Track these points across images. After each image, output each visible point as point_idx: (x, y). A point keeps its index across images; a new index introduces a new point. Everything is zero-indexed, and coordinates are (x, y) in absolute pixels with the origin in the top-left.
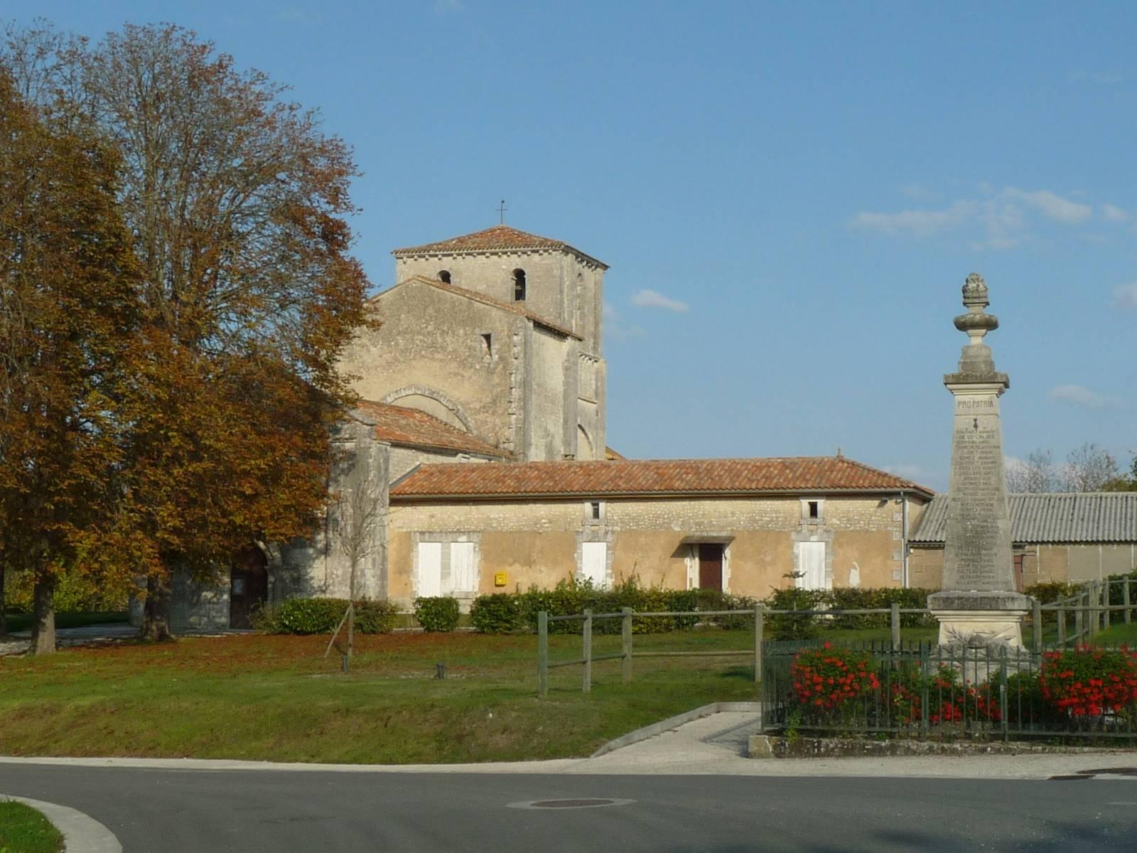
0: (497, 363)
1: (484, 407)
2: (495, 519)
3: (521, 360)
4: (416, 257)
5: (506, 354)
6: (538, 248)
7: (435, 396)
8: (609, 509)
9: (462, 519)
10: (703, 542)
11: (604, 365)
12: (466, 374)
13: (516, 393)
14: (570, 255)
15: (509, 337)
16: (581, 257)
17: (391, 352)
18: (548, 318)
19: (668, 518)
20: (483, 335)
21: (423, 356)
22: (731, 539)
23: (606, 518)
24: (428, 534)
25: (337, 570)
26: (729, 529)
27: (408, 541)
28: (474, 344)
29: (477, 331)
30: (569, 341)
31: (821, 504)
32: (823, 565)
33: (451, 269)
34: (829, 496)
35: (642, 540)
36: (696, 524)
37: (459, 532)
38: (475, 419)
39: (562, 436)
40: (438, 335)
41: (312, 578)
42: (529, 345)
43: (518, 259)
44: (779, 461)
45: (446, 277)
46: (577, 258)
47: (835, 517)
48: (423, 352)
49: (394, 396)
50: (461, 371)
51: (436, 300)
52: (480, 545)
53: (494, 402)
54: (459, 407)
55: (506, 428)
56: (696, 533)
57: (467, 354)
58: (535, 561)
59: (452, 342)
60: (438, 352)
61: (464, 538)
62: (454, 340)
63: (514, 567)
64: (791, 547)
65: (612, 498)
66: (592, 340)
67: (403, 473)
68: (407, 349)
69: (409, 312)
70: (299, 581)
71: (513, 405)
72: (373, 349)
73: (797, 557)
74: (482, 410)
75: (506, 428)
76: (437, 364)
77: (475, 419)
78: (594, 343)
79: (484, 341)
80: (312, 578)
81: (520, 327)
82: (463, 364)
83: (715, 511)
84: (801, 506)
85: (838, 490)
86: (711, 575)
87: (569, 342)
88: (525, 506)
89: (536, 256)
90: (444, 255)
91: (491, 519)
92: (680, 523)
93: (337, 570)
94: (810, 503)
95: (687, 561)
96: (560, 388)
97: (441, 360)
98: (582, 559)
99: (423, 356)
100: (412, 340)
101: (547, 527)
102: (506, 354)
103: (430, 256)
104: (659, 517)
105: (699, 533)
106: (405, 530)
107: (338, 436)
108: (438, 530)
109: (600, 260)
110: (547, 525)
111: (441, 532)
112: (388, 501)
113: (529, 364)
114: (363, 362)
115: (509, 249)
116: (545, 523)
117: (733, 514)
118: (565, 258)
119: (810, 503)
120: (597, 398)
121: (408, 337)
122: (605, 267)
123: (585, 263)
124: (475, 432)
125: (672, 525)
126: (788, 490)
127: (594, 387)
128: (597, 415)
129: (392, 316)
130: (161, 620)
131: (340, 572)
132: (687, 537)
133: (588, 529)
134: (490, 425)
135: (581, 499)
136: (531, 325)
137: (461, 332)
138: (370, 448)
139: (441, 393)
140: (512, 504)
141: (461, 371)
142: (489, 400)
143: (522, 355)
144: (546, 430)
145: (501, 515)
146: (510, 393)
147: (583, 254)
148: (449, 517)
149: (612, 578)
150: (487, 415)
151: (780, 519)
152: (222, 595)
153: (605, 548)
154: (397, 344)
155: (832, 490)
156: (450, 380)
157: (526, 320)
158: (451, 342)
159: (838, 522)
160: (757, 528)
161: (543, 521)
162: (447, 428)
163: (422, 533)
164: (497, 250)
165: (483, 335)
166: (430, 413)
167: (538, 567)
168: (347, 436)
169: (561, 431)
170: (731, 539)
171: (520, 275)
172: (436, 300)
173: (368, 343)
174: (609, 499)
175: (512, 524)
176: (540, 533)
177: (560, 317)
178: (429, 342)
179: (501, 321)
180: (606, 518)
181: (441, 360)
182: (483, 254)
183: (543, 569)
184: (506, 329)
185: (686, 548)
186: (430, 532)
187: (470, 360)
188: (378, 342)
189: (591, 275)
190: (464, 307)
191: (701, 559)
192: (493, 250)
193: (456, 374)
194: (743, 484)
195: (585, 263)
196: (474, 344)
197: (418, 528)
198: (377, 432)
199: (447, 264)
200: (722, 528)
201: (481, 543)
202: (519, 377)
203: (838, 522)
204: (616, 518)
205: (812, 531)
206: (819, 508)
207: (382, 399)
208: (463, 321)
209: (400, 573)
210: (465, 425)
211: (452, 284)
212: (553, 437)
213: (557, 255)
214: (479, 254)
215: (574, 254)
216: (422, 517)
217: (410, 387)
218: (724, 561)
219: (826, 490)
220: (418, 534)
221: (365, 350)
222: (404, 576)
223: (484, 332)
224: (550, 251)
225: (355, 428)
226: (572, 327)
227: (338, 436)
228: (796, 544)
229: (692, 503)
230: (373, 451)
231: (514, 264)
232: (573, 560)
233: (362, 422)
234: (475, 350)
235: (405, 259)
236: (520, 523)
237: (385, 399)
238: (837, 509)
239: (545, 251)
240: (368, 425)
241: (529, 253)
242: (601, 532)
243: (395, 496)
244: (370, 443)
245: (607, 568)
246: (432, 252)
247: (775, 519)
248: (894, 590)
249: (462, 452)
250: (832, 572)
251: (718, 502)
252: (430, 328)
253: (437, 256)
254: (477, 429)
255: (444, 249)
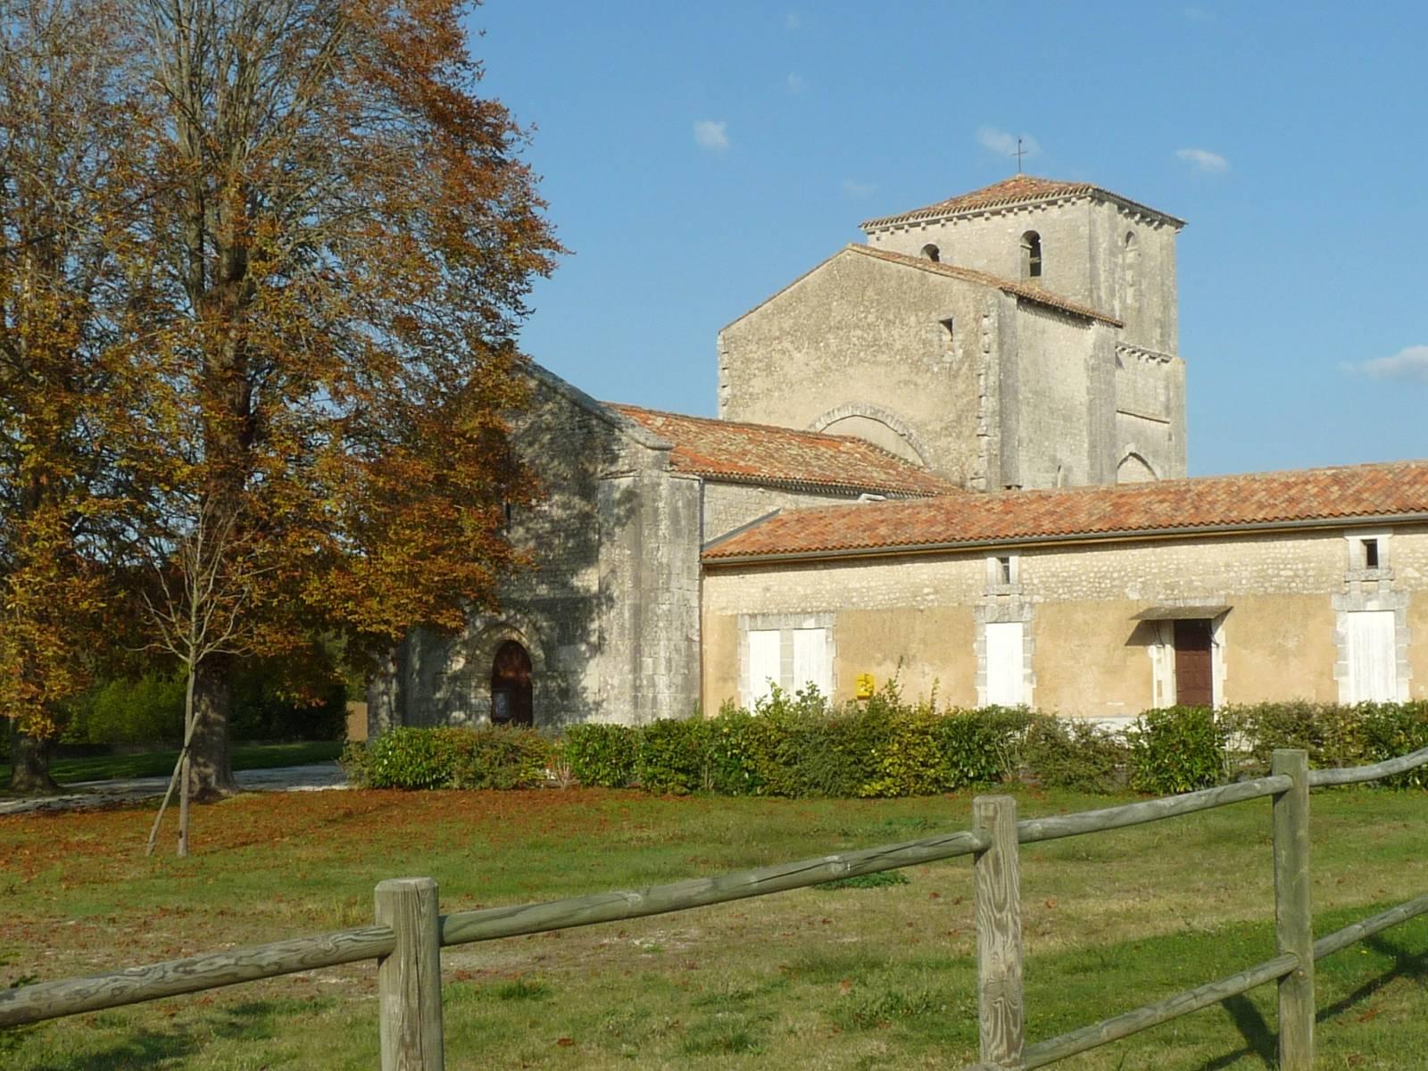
0: (962, 362)
1: (946, 429)
2: (855, 590)
3: (994, 354)
4: (892, 229)
5: (973, 347)
6: (1055, 197)
7: (879, 416)
8: (1025, 566)
9: (809, 592)
10: (1154, 617)
11: (1181, 366)
12: (919, 381)
13: (989, 404)
14: (1107, 204)
15: (977, 320)
16: (1127, 207)
17: (819, 358)
18: (1072, 298)
19: (1120, 578)
20: (942, 322)
21: (862, 360)
22: (1224, 613)
23: (1020, 581)
24: (761, 618)
25: (612, 677)
26: (1222, 593)
27: (734, 630)
28: (929, 336)
29: (934, 316)
30: (1096, 326)
31: (1384, 541)
32: (1392, 653)
33: (939, 241)
34: (1399, 527)
35: (1079, 617)
36: (1166, 586)
37: (804, 612)
38: (934, 447)
39: (1087, 468)
40: (882, 327)
41: (585, 689)
42: (1009, 331)
43: (1029, 218)
44: (1329, 472)
45: (933, 252)
46: (1121, 208)
47: (1411, 565)
48: (862, 354)
49: (825, 420)
50: (915, 378)
51: (878, 277)
52: (835, 632)
53: (959, 420)
54: (912, 431)
55: (975, 457)
56: (1164, 601)
57: (921, 351)
58: (914, 656)
59: (901, 336)
60: (883, 353)
61: (810, 623)
62: (903, 333)
63: (883, 667)
64: (1331, 622)
65: (1030, 548)
66: (1159, 331)
67: (738, 525)
68: (840, 351)
69: (842, 298)
70: (568, 696)
71: (983, 422)
72: (797, 355)
73: (1343, 640)
74: (944, 432)
75: (975, 457)
76: (882, 370)
77: (934, 447)
78: (1162, 335)
79: (946, 330)
80: (585, 689)
81: (992, 305)
82: (916, 365)
83: (1196, 562)
84: (1347, 549)
85: (1412, 514)
86: (1194, 681)
87: (1094, 332)
88: (899, 567)
89: (1054, 210)
90: (928, 223)
91: (849, 591)
92: (1139, 585)
93: (612, 677)
94: (1364, 541)
95: (1153, 650)
96: (1082, 397)
97: (887, 364)
98: (985, 652)
99: (862, 360)
100: (848, 338)
101: (932, 601)
102: (973, 347)
103: (911, 225)
104: (1104, 577)
105: (1171, 603)
106: (730, 613)
107: (613, 469)
108: (775, 611)
109: (1165, 213)
110: (932, 597)
111: (779, 614)
112: (697, 569)
113: (1009, 359)
114: (785, 375)
115: (1016, 204)
116: (928, 594)
117: (1227, 565)
118: (1098, 208)
119: (1364, 541)
120: (1168, 414)
121: (841, 333)
122: (1179, 224)
123: (1137, 217)
124: (934, 466)
125: (1127, 590)
126: (1321, 520)
127: (1162, 398)
128: (1170, 439)
129: (820, 306)
130: (206, 766)
131: (616, 682)
132: (1150, 610)
133: (993, 602)
134: (955, 454)
135: (982, 551)
136: (1013, 301)
137: (913, 318)
138: (659, 485)
139: (888, 412)
140: (879, 564)
141: (915, 378)
142: (952, 417)
143: (995, 347)
144: (1053, 459)
145: (865, 584)
146: (979, 404)
147: (1131, 203)
148: (790, 589)
149: (1031, 682)
150: (950, 439)
151: (1311, 573)
152: (477, 717)
153: (1021, 632)
154: (827, 345)
155: (1400, 515)
156: (899, 391)
157: (1002, 294)
158: (897, 337)
159: (1417, 575)
160: (1271, 590)
161: (926, 590)
162: (891, 461)
163: (753, 616)
164: (999, 207)
165: (942, 322)
166: (874, 442)
167: (920, 665)
168: (626, 468)
169: (1086, 462)
170: (1224, 613)
171: (1033, 239)
172: (878, 277)
173: (790, 347)
174: (1023, 549)
175: (880, 597)
176: (922, 611)
177: (1091, 296)
178: (870, 338)
179: (964, 298)
180: (1020, 581)
181: (887, 364)
182: (981, 214)
183: (927, 669)
184: (972, 308)
185: (1149, 629)
186: (764, 615)
187: (925, 360)
188: (803, 345)
189: (1154, 239)
190: (915, 284)
191: (1178, 647)
192: (994, 207)
193: (907, 383)
194: (1252, 513)
195: (1137, 217)
196: (929, 336)
197: (747, 608)
198: (668, 457)
199: (934, 234)
200: (1210, 593)
201: (836, 630)
202: (992, 379)
203: (1417, 575)
204: (1036, 581)
205: (1369, 593)
206: (1379, 551)
207: (810, 427)
208: (914, 303)
209: (725, 680)
210: (920, 456)
211: (941, 261)
212: (1069, 469)
213: (1084, 204)
214: (975, 216)
215: (1115, 202)
216: (753, 590)
217: (845, 406)
218: (1214, 650)
219: (1388, 516)
220: (747, 617)
221: (786, 357)
222: (730, 684)
223: (943, 318)
224: (1074, 199)
225: (636, 453)
226: (1113, 310)
227: (613, 469)
228: (1342, 617)
229: (1159, 550)
230: (664, 490)
231: (1024, 225)
232: (971, 653)
233: (644, 445)
234: (932, 346)
235: (878, 232)
236: (892, 596)
237: (813, 425)
238: (1413, 551)
239: (1067, 201)
240: (653, 449)
241: (1043, 206)
242: (1014, 606)
243: (709, 560)
244: (659, 477)
245: (1025, 666)
246: (912, 220)
247: (1301, 573)
248: (1386, 707)
249: (869, 492)
250: (1408, 665)
251: (1201, 546)
252: (871, 318)
253: (918, 225)
254: (938, 461)
255: (931, 216)
